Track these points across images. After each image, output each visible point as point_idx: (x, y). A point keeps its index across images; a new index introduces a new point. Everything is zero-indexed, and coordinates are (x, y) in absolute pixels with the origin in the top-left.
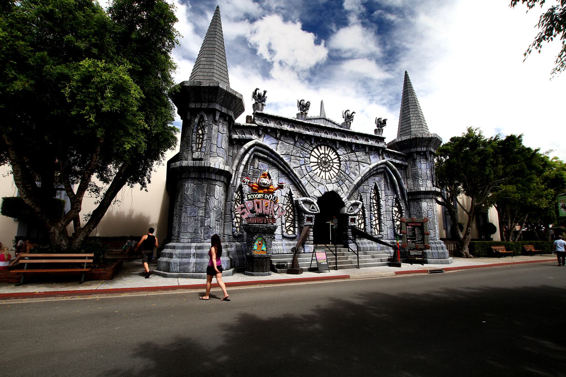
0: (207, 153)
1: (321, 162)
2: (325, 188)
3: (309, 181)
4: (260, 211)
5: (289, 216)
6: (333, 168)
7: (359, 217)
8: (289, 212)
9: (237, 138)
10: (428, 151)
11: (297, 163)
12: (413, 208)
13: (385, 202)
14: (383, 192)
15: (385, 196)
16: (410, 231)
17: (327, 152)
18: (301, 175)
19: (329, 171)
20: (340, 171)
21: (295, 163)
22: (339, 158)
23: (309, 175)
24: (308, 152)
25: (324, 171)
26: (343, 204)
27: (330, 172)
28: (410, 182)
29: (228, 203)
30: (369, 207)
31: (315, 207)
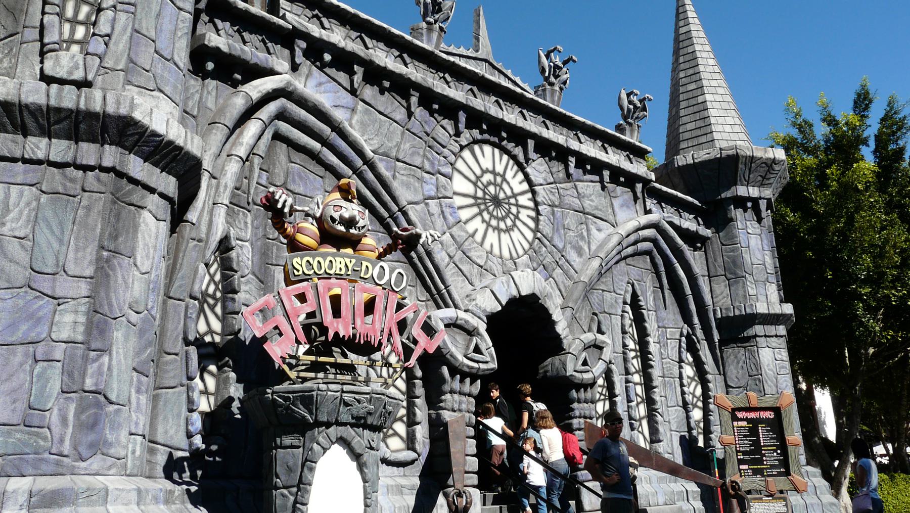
0: (116, 63)
2: (508, 283)
3: (451, 257)
4: (346, 328)
6: (518, 223)
9: (225, 49)
10: (764, 198)
11: (415, 190)
12: (736, 368)
15: (659, 327)
16: (745, 436)
17: (500, 169)
19: (508, 230)
20: (539, 235)
22: (534, 193)
24: (445, 157)
25: (494, 229)
26: (556, 346)
27: (511, 233)
28: (721, 287)
29: (175, 306)
30: (621, 360)
31: (483, 347)
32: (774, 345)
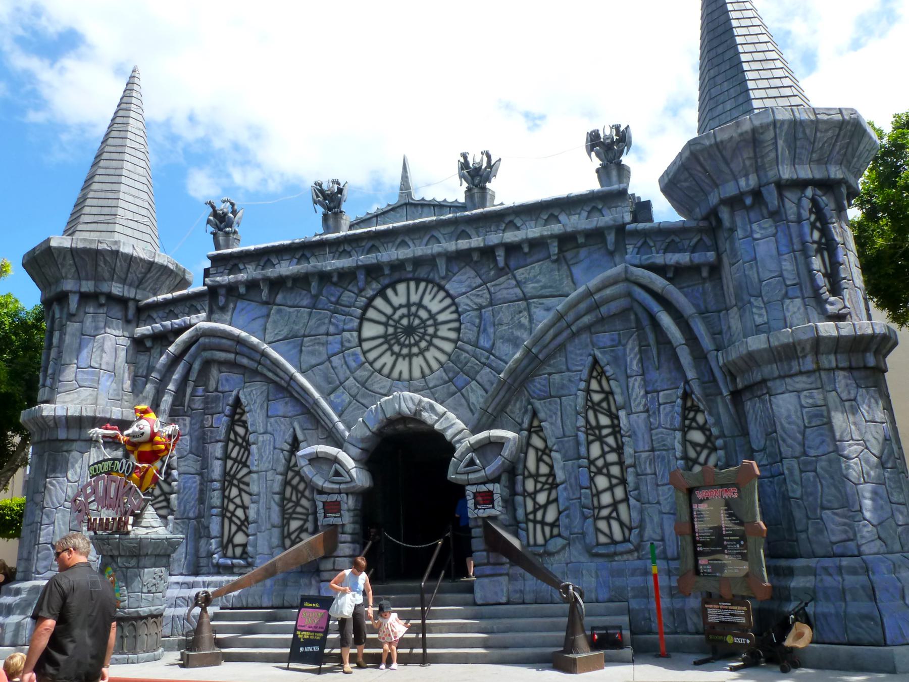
1: (395, 333)
5: (298, 500)
7: (536, 482)
8: (298, 491)
10: (768, 184)
11: (320, 353)
13: (644, 415)
14: (636, 384)
15: (647, 392)
18: (330, 383)
21: (312, 353)
23: (355, 379)
32: (799, 386)
